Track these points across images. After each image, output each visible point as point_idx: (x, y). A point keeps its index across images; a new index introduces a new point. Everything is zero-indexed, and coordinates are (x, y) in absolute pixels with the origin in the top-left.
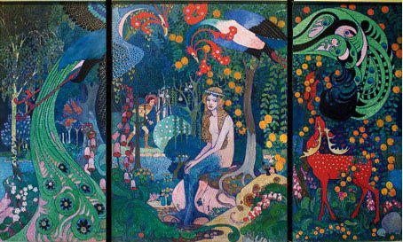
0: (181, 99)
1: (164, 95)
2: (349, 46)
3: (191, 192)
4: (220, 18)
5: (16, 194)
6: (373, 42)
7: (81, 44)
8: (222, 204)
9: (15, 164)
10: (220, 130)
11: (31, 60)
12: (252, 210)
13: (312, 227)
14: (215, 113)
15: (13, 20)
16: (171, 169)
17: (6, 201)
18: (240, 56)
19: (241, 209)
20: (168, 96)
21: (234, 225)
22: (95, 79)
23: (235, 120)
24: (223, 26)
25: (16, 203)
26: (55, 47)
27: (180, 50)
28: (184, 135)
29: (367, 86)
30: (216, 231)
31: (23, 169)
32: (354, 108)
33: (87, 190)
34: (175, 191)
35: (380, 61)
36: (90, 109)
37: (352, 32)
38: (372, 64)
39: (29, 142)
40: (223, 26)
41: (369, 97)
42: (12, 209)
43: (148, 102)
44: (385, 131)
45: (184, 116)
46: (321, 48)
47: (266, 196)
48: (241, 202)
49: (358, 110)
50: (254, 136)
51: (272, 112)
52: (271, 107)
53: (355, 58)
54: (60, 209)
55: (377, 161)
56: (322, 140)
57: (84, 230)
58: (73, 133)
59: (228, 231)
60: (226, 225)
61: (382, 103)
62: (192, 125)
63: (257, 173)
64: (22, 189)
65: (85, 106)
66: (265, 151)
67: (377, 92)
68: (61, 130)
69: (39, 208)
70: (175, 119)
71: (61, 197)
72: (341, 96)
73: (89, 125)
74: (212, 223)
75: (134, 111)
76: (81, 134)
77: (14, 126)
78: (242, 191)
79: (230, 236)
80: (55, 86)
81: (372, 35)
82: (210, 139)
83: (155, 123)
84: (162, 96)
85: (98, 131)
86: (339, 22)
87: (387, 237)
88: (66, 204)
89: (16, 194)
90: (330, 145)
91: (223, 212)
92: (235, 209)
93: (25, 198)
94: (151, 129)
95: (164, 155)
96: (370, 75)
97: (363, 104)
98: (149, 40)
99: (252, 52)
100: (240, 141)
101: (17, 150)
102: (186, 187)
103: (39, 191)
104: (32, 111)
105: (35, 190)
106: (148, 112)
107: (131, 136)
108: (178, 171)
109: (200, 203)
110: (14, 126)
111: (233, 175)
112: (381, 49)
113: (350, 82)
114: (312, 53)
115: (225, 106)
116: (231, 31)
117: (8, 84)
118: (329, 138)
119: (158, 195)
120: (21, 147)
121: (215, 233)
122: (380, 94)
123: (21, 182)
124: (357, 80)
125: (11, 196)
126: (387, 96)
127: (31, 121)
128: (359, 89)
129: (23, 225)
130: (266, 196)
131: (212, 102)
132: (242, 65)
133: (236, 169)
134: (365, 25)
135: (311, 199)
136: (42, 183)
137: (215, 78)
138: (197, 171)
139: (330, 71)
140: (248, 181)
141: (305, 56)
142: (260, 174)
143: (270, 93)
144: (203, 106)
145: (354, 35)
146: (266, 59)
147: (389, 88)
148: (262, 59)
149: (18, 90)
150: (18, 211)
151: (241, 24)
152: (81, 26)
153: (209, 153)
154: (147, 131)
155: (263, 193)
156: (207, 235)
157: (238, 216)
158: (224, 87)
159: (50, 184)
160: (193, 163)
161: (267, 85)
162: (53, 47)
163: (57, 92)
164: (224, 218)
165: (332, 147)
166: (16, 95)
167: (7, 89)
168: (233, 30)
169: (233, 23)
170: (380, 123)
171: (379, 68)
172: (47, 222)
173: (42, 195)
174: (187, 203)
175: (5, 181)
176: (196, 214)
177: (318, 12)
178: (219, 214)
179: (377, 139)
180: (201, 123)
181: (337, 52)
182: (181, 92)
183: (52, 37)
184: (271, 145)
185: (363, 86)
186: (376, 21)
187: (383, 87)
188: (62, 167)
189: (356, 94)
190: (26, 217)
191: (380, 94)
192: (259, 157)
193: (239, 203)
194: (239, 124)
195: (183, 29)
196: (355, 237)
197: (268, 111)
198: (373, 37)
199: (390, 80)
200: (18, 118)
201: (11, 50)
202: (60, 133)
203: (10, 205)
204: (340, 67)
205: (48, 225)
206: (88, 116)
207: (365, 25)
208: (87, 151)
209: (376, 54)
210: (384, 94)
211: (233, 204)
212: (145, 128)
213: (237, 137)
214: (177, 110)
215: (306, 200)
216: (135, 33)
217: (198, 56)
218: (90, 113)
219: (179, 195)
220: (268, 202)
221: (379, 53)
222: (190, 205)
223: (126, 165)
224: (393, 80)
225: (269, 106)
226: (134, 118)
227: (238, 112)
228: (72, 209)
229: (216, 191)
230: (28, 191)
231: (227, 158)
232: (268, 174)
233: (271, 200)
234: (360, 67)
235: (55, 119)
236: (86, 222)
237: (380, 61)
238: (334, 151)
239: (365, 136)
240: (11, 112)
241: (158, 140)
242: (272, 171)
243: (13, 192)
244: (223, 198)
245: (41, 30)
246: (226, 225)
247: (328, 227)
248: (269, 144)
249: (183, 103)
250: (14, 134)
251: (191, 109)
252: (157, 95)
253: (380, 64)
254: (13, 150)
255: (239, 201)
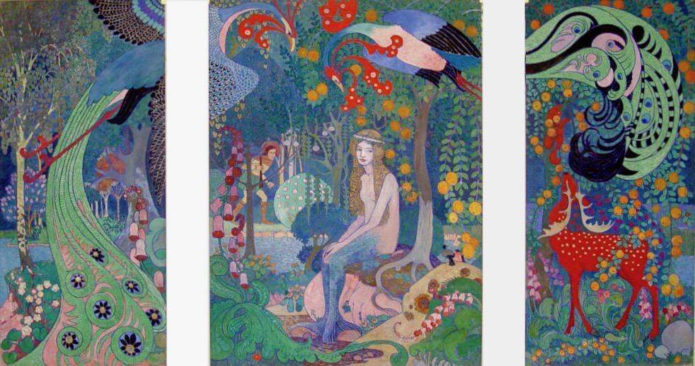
0: (316, 148)
1: (290, 142)
2: (614, 66)
3: (334, 292)
4: (377, 22)
5: (25, 295)
6: (650, 59)
7: (121, 65)
8: (382, 309)
9: (23, 250)
10: (377, 195)
11: (47, 89)
12: (427, 319)
13: (556, 344)
14: (369, 169)
15: (16, 29)
16: (302, 256)
17: (11, 306)
18: (408, 82)
19: (409, 316)
20: (296, 144)
21: (400, 342)
22: (144, 119)
23: (400, 180)
24: (381, 35)
25: (28, 309)
26: (80, 69)
27: (314, 73)
28: (322, 204)
29: (641, 128)
30: (371, 351)
31: (36, 256)
32: (622, 161)
33: (134, 289)
34: (309, 290)
35: (660, 88)
36: (137, 164)
37: (618, 44)
38: (649, 94)
39: (43, 215)
40: (381, 35)
41: (644, 144)
42: (19, 317)
43: (266, 154)
44: (668, 196)
45: (319, 173)
46: (571, 68)
47: (448, 298)
48: (411, 307)
49: (628, 163)
50: (430, 205)
51: (457, 169)
52: (456, 160)
53: (622, 83)
54: (94, 317)
55: (655, 243)
56: (573, 211)
57: (130, 349)
58: (112, 203)
59: (389, 350)
60: (388, 342)
61: (664, 153)
62: (334, 189)
63: (435, 262)
64: (34, 287)
65: (130, 160)
66: (446, 228)
67: (656, 136)
68: (92, 196)
69: (62, 316)
70: (308, 178)
71: (94, 300)
72: (602, 142)
73: (136, 189)
74: (366, 338)
75: (244, 167)
76: (124, 203)
77: (20, 192)
78: (412, 288)
79: (395, 359)
80: (82, 130)
81: (649, 47)
82: (362, 205)
83: (277, 187)
84: (287, 143)
85: (150, 200)
86: (597, 29)
87: (670, 358)
88: (103, 310)
89: (25, 295)
90: (585, 218)
91: (383, 322)
92: (401, 317)
93: (39, 301)
94: (271, 195)
95: (291, 235)
96: (645, 109)
97: (634, 155)
98: (266, 57)
99: (430, 76)
100: (408, 211)
101: (26, 227)
102: (326, 284)
103: (60, 290)
104: (48, 168)
105: (55, 288)
106: (266, 168)
107: (239, 205)
108: (312, 259)
109: (347, 309)
110: (20, 192)
111: (398, 265)
112: (662, 71)
113: (614, 121)
114: (557, 76)
115: (384, 158)
116: (394, 43)
117: (11, 126)
118: (582, 207)
119: (283, 296)
120: (33, 224)
121: (370, 354)
122: (661, 139)
123: (33, 276)
124: (626, 118)
125: (17, 298)
126: (670, 142)
127: (46, 183)
128: (628, 132)
129: (37, 343)
130: (448, 298)
131: (365, 152)
132: (411, 95)
133: (402, 256)
134: (638, 33)
135: (555, 301)
136: (66, 278)
137: (370, 115)
138: (344, 259)
139: (585, 105)
140: (421, 270)
141: (546, 81)
142: (440, 263)
143: (454, 138)
144: (351, 159)
145: (622, 47)
146: (447, 85)
147: (675, 131)
148: (441, 85)
149: (26, 136)
150: (28, 320)
151: (409, 30)
152: (122, 37)
153: (361, 231)
154: (264, 198)
155: (444, 292)
156: (357, 358)
157: (406, 328)
158: (383, 130)
159: (78, 279)
160: (335, 247)
161: (450, 125)
162: (79, 69)
163: (86, 139)
164: (385, 331)
165: (588, 222)
166: (23, 143)
167: (8, 134)
168: (397, 41)
169: (397, 30)
170: (660, 185)
171: (658, 99)
172: (74, 337)
173: (66, 296)
174: (327, 309)
175: (9, 274)
176: (340, 325)
177: (566, 13)
178: (376, 325)
179: (656, 209)
180: (348, 185)
181: (596, 75)
182: (317, 138)
183: (78, 54)
184: (456, 219)
185: (635, 126)
186: (655, 26)
187: (665, 128)
188: (96, 254)
189: (624, 140)
190: (44, 327)
191: (661, 139)
192: (438, 237)
193: (407, 309)
194: (407, 186)
195: (320, 39)
196: (621, 360)
197: (452, 166)
198: (651, 51)
199: (677, 118)
200: (27, 179)
201: (15, 75)
202: (91, 202)
203: (15, 313)
204: (599, 97)
205: (75, 342)
206: (136, 176)
207: (638, 33)
208: (133, 229)
209: (655, 77)
210: (666, 140)
211: (399, 309)
212: (261, 193)
213: (403, 207)
214: (313, 164)
215: (548, 302)
216: (244, 46)
217: (342, 81)
218: (138, 171)
219: (314, 297)
220: (452, 307)
221: (660, 76)
222: (331, 312)
223: (233, 251)
224: (681, 117)
225: (452, 158)
226: (244, 178)
227: (405, 169)
228: (112, 318)
229: (370, 290)
230: (45, 290)
231: (388, 240)
232: (452, 263)
233: (457, 303)
234: (630, 97)
235: (84, 181)
236: (133, 337)
237: (660, 88)
238: (590, 227)
239: (638, 204)
240: (14, 168)
241: (281, 212)
242: (457, 259)
243: (21, 291)
244: (382, 300)
245: (60, 43)
246: (388, 342)
247: (580, 344)
248: (452, 218)
249: (321, 154)
250: (21, 203)
251: (333, 164)
252: (279, 140)
253: (662, 93)
254: (20, 228)
255: (406, 305)
